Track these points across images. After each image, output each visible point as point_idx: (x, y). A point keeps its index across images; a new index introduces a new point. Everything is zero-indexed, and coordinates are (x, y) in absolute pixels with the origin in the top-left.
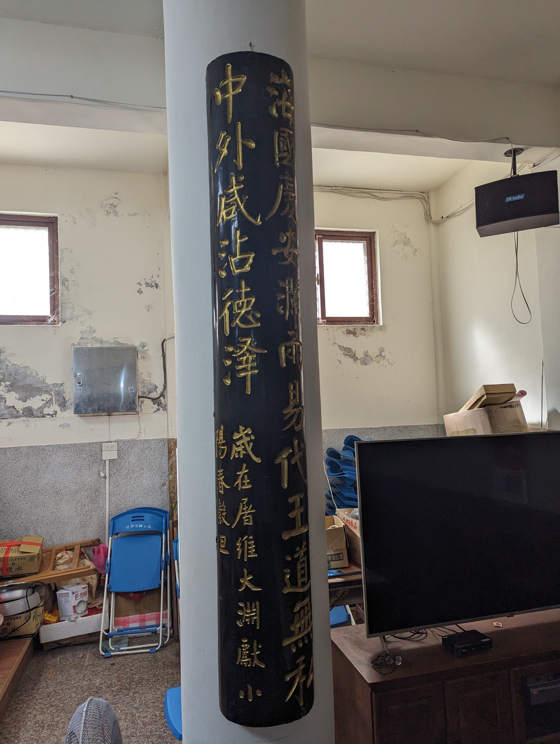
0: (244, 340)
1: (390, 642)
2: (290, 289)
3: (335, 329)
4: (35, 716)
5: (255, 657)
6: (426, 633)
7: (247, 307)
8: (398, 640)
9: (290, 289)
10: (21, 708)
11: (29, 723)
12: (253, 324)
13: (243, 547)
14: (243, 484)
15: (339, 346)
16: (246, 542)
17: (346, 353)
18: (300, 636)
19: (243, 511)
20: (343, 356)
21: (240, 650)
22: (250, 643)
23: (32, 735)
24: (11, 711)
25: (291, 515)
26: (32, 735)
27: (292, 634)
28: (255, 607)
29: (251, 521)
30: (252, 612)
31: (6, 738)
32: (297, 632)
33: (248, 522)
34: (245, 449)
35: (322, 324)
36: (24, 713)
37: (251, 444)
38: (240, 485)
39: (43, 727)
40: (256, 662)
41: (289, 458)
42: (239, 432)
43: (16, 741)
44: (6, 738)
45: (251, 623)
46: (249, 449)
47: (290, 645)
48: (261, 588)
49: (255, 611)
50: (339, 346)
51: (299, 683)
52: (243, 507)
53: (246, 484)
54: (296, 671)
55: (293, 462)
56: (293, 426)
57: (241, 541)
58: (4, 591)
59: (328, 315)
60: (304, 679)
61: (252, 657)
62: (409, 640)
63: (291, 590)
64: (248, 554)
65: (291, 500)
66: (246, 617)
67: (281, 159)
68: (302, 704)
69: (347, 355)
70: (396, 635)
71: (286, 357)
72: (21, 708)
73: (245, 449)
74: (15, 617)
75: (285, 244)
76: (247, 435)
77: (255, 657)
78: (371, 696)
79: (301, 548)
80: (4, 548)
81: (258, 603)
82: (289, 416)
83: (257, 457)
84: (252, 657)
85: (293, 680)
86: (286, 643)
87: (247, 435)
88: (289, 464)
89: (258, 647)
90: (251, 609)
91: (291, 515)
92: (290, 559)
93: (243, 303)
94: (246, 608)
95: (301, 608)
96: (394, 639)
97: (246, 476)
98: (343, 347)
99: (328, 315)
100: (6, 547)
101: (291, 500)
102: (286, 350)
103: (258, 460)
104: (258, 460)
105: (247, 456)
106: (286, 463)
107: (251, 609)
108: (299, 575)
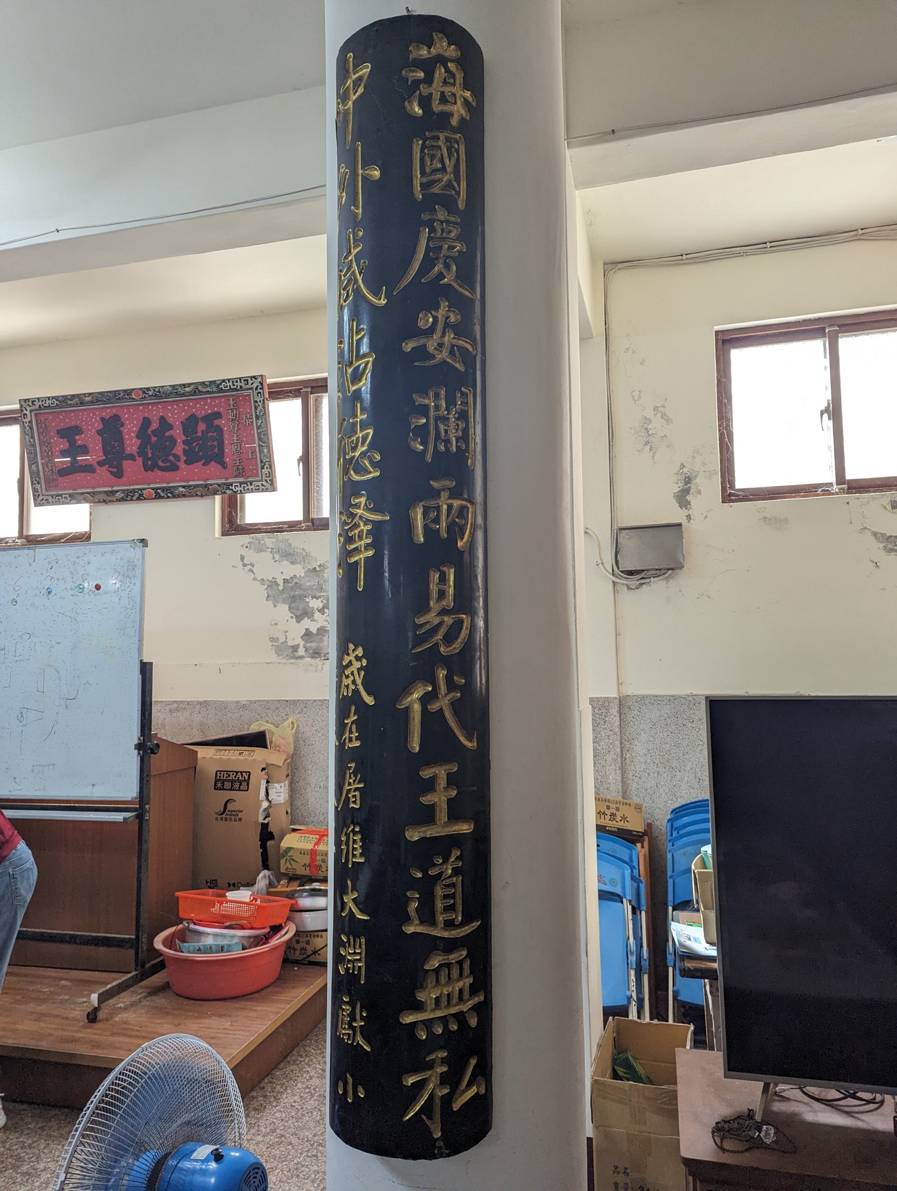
0: (357, 501)
1: (788, 1099)
2: (437, 407)
3: (865, 500)
4: (311, 1078)
5: (358, 1030)
6: (882, 1102)
7: (363, 444)
8: (807, 1099)
9: (437, 407)
10: (301, 1062)
11: (299, 1085)
12: (370, 472)
13: (347, 844)
14: (351, 740)
15: (875, 534)
16: (351, 834)
17: (890, 546)
18: (439, 1014)
19: (350, 784)
20: (883, 552)
21: (340, 1012)
22: (352, 1003)
23: (295, 1102)
24: (289, 1062)
25: (426, 799)
26: (295, 1102)
27: (418, 1007)
28: (360, 947)
29: (358, 802)
30: (355, 953)
31: (265, 1096)
32: (431, 1005)
33: (354, 802)
34: (354, 682)
35: (837, 493)
36: (301, 1070)
37: (362, 673)
38: (347, 741)
39: (312, 1095)
40: (359, 1038)
41: (425, 700)
42: (348, 655)
43: (274, 1104)
44: (265, 1096)
45: (353, 970)
46: (359, 681)
47: (413, 1025)
48: (369, 915)
49: (360, 954)
50: (875, 534)
51: (432, 1096)
52: (350, 778)
53: (354, 739)
54: (430, 1072)
55: (434, 707)
56: (436, 645)
57: (346, 834)
58: (305, 894)
59: (850, 475)
60: (446, 1091)
61: (353, 1029)
62: (830, 1106)
63: (420, 929)
64: (354, 856)
65: (426, 773)
66: (349, 961)
67: (424, 186)
68: (438, 1135)
69: (892, 550)
70: (810, 1089)
71: (426, 527)
72: (301, 1062)
73: (354, 682)
74: (316, 934)
75: (432, 330)
76: (358, 659)
77: (358, 1030)
78: (687, 1182)
79: (446, 861)
80: (315, 836)
81: (363, 940)
82: (428, 627)
83: (369, 694)
84: (353, 1029)
85: (420, 1086)
86: (408, 1019)
87: (358, 659)
88: (424, 711)
89: (361, 1015)
90: (355, 948)
91: (426, 799)
92: (420, 875)
93: (358, 439)
94: (349, 946)
95: (441, 966)
96: (798, 1094)
97: (354, 727)
98: (883, 535)
99: (850, 475)
100: (318, 837)
101: (426, 773)
102: (425, 514)
103: (369, 700)
104: (369, 700)
105: (356, 692)
106: (417, 707)
107: (355, 948)
108: (439, 905)
